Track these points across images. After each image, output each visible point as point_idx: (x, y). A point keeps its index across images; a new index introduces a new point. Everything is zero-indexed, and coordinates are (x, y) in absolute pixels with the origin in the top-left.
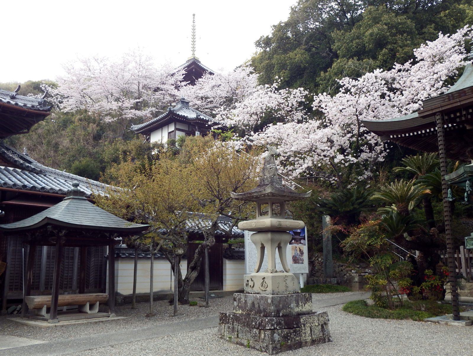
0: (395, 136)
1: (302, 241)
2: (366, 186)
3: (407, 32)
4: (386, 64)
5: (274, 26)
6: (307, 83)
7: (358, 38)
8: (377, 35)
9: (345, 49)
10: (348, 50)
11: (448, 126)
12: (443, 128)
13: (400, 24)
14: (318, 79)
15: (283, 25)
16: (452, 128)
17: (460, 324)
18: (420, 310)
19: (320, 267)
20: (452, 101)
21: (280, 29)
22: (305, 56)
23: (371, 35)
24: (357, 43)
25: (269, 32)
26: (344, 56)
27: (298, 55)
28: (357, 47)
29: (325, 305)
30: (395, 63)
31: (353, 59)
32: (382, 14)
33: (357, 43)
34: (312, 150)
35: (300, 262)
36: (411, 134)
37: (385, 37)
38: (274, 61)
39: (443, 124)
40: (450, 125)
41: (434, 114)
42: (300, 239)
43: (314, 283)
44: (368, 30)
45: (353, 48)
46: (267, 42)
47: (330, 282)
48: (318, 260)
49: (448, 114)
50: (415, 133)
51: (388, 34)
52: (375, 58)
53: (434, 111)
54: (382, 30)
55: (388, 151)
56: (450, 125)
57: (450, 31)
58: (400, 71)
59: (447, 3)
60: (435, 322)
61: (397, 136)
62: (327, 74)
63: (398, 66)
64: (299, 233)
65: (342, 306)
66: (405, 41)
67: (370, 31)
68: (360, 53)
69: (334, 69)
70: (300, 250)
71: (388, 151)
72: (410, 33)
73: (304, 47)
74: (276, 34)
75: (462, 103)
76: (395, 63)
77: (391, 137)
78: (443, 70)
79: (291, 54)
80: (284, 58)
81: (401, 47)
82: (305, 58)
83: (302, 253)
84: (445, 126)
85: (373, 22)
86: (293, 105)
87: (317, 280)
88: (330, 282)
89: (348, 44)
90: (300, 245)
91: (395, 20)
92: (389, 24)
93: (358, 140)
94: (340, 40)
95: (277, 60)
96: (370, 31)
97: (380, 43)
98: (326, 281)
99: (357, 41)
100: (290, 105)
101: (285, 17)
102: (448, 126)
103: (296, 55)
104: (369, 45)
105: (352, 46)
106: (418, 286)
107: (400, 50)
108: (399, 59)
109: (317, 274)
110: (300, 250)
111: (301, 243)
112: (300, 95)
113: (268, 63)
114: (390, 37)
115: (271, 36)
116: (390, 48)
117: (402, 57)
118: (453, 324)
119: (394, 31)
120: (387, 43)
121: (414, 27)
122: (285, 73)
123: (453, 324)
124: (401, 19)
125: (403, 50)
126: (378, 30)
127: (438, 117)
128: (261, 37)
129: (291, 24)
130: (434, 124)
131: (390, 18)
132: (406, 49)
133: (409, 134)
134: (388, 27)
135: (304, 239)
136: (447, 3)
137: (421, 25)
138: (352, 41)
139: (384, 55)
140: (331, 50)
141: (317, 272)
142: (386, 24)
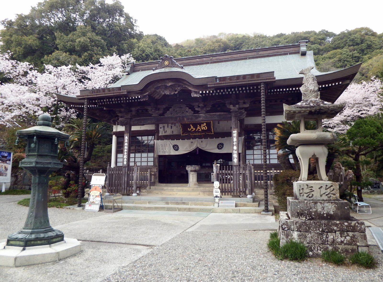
0: (74, 106)
1: (8, 162)
2: (15, 134)
3: (101, 46)
4: (86, 62)
5: (17, 15)
6: (37, 60)
7: (72, 41)
8: (83, 43)
9: (62, 46)
10: (64, 46)
11: (90, 106)
12: (87, 107)
13: (97, 41)
14: (42, 59)
15: (23, 16)
16: (94, 108)
17: (80, 209)
18: (64, 202)
19: (21, 179)
20: (94, 94)
21: (21, 18)
22: (36, 42)
23: (80, 42)
24: (70, 44)
25: (13, 18)
26: (61, 50)
27: (31, 40)
28: (70, 47)
29: (9, 201)
30: (90, 63)
31: (66, 53)
32: (88, 32)
33: (70, 44)
34: (21, 106)
35: (4, 175)
36: (80, 106)
37: (87, 46)
38: (13, 39)
39: (88, 105)
40: (93, 106)
41: (84, 99)
42: (7, 161)
43: (14, 189)
44: (78, 38)
45: (68, 47)
46: (10, 24)
47: (25, 188)
48: (20, 174)
49: (91, 100)
50: (80, 106)
51: (89, 44)
52: (80, 56)
53: (84, 97)
54: (87, 41)
55: (77, 113)
56: (93, 106)
57: (120, 53)
58: (92, 68)
59: (126, 37)
60: (68, 208)
61: (75, 106)
62: (48, 58)
63: (91, 65)
64: (6, 157)
65: (16, 202)
66: (98, 52)
67: (79, 39)
68: (71, 51)
69: (53, 56)
70: (5, 167)
71: (77, 113)
72: (102, 48)
73: (36, 36)
74: (18, 21)
75: (97, 96)
76: (90, 63)
77: (72, 106)
78: (111, 74)
79: (25, 38)
80: (21, 39)
81: (95, 54)
82: (36, 43)
83: (6, 169)
84: (89, 106)
85: (82, 34)
86: (20, 72)
87: (16, 187)
88: (25, 188)
89: (65, 43)
90: (5, 164)
91: (95, 37)
92: (91, 39)
93: (57, 103)
94: (61, 39)
95: (15, 38)
96: (79, 39)
97: (84, 48)
98: (22, 188)
99: (71, 43)
100: (18, 72)
101: (26, 12)
102: (90, 106)
103: (29, 40)
104: (78, 47)
105: (67, 45)
106: (65, 190)
107: (95, 56)
108: (93, 61)
109: (19, 183)
110: (5, 167)
111: (6, 163)
112: (25, 67)
113: (9, 39)
114: (90, 47)
115: (13, 20)
116: (89, 53)
117: (96, 60)
118: (76, 209)
119: (93, 44)
120: (88, 50)
121: (105, 45)
122: (20, 49)
123: (76, 209)
124: (99, 38)
125: (97, 56)
126: (84, 40)
127: (85, 101)
128: (6, 20)
129: (31, 17)
130: (83, 104)
131: (92, 36)
132: (98, 56)
133: (81, 106)
134: (90, 40)
135: (10, 160)
136: (126, 37)
137: (110, 45)
138: (67, 42)
139: (85, 56)
140: (54, 43)
141: (19, 182)
142: (89, 38)
